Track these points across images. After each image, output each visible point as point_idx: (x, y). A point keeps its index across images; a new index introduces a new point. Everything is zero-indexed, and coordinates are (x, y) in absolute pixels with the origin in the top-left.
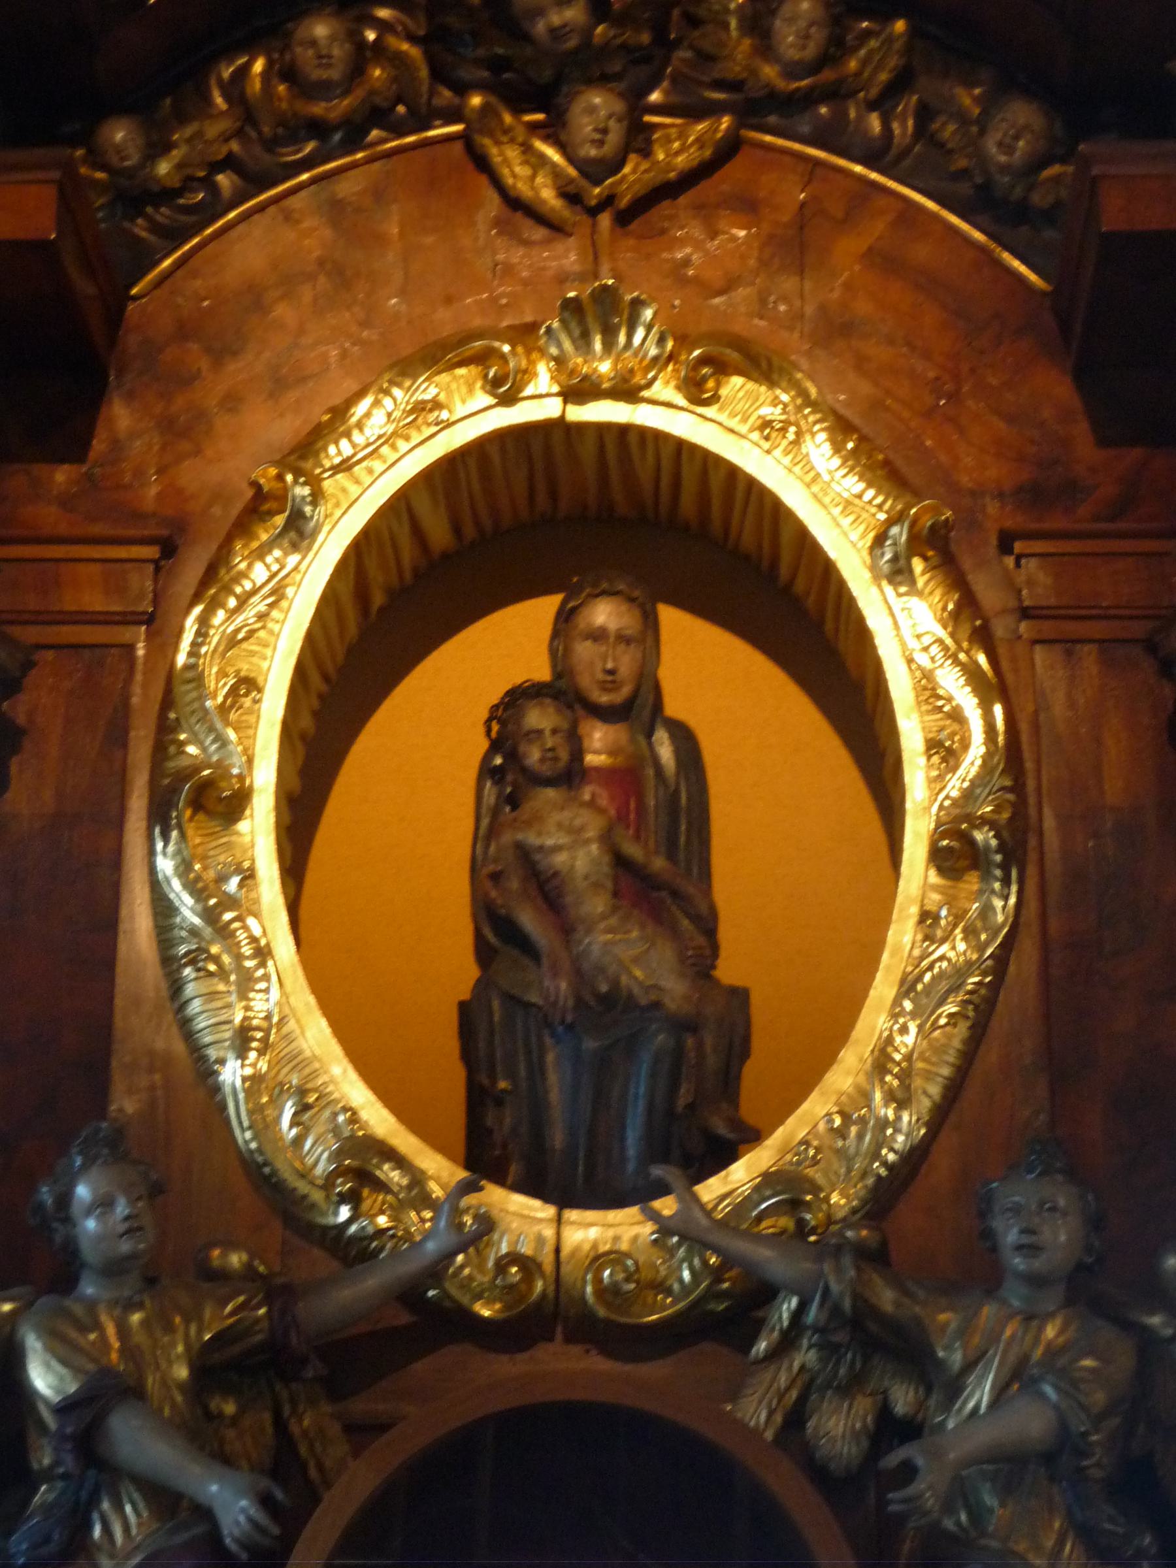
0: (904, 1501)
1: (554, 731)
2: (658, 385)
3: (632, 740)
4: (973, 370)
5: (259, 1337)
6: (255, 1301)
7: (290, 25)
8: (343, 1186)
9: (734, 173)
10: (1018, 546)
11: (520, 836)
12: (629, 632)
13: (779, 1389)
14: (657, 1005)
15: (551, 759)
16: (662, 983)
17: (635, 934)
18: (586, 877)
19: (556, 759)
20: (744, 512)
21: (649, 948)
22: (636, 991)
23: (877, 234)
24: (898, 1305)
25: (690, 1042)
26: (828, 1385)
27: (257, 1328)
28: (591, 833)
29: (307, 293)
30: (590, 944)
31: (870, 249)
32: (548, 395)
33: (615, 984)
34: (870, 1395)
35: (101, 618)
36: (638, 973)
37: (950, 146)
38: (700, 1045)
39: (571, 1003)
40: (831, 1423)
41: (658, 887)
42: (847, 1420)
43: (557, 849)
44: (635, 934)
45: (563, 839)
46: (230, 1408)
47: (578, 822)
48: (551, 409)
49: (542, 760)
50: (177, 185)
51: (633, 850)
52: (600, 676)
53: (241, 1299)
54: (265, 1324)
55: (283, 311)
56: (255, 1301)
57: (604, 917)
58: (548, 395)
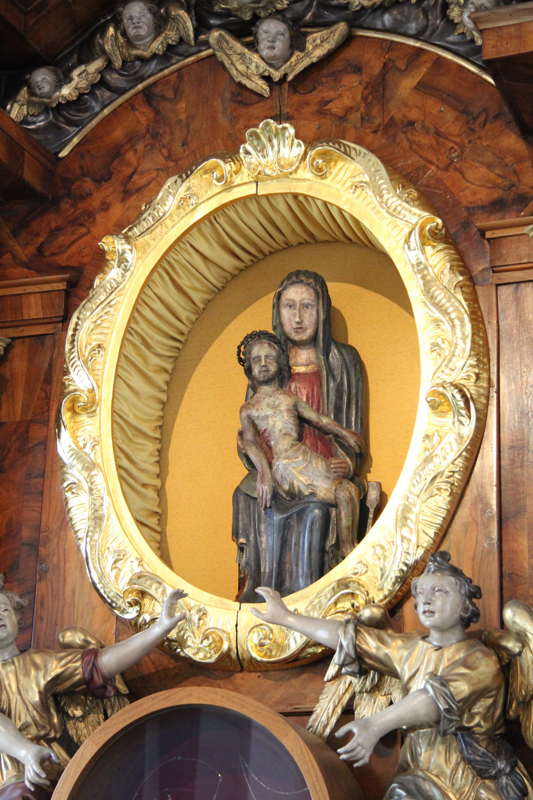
0: (346, 752)
1: (267, 357)
2: (300, 171)
3: (318, 358)
4: (470, 142)
5: (78, 677)
6: (76, 658)
7: (121, 9)
8: (131, 598)
9: (351, 53)
10: (488, 235)
11: (249, 412)
12: (306, 301)
13: (339, 695)
14: (313, 494)
15: (265, 371)
16: (315, 483)
17: (300, 458)
18: (280, 431)
19: (267, 371)
20: (335, 233)
21: (307, 465)
22: (302, 488)
23: (422, 74)
24: (378, 648)
25: (333, 513)
26: (361, 692)
27: (77, 672)
28: (283, 408)
29: (140, 147)
30: (278, 465)
31: (420, 83)
32: (251, 182)
33: (292, 485)
34: (385, 695)
35: (36, 321)
36: (302, 479)
37: (456, 21)
38: (338, 515)
39: (269, 497)
40: (365, 711)
41: (327, 433)
42: (373, 709)
43: (266, 417)
44: (300, 458)
45: (269, 412)
46: (78, 713)
47: (277, 402)
48: (250, 190)
49: (260, 372)
50: (75, 99)
51: (310, 414)
52: (295, 326)
53: (70, 658)
54: (80, 670)
55: (130, 156)
56: (76, 658)
57: (286, 450)
58: (251, 182)
